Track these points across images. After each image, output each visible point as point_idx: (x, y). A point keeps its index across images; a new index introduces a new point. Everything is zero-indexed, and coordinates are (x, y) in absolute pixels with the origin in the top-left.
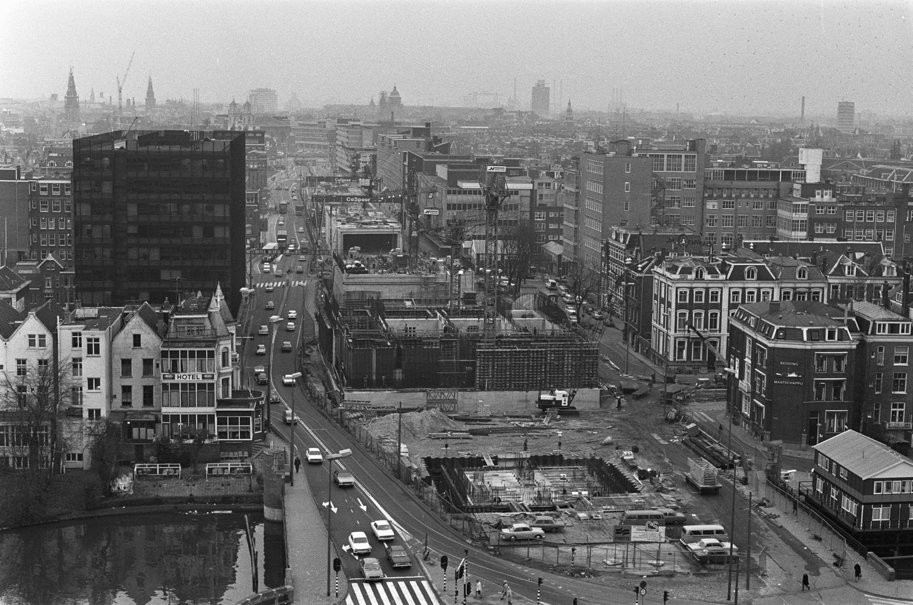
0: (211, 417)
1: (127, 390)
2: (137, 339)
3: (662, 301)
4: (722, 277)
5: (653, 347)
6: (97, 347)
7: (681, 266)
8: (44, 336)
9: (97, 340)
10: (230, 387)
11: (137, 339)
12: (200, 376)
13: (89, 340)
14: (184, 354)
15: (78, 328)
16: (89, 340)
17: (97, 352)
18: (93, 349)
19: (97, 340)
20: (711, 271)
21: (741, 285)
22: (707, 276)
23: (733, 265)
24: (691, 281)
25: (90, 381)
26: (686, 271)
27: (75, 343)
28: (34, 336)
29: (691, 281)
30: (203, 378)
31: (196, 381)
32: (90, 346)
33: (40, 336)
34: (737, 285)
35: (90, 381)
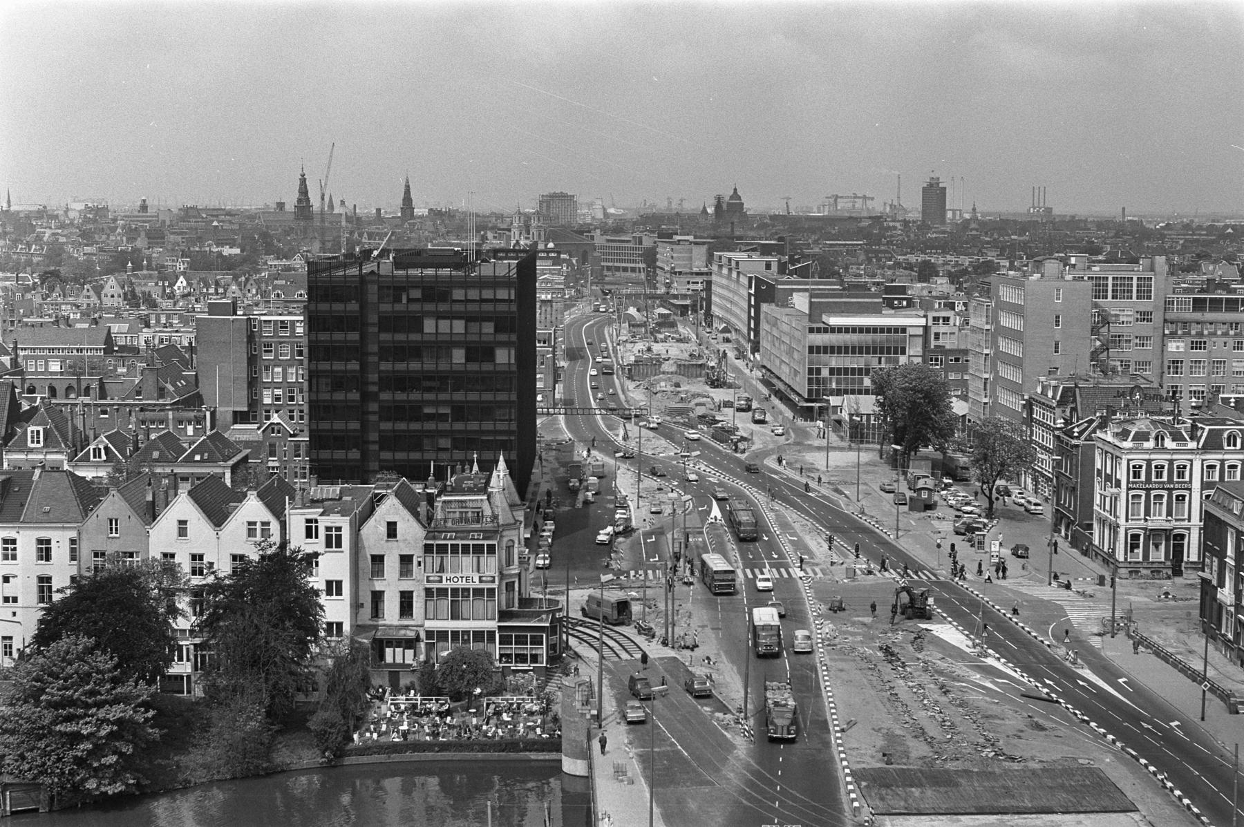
0: (491, 634)
1: (377, 597)
2: (392, 529)
3: (1108, 478)
4: (1192, 445)
5: (1096, 543)
6: (339, 538)
7: (1134, 430)
8: (268, 524)
9: (339, 529)
10: (517, 594)
11: (392, 529)
12: (476, 579)
13: (328, 529)
14: (455, 549)
15: (314, 513)
16: (328, 529)
17: (339, 545)
18: (333, 541)
19: (339, 529)
20: (1177, 437)
21: (1220, 457)
22: (1169, 444)
23: (1207, 428)
24: (1147, 451)
25: (330, 625)
26: (1141, 437)
27: (310, 533)
28: (255, 523)
29: (1147, 451)
30: (481, 581)
31: (471, 586)
32: (329, 538)
33: (263, 524)
34: (1213, 458)
35: (329, 583)
